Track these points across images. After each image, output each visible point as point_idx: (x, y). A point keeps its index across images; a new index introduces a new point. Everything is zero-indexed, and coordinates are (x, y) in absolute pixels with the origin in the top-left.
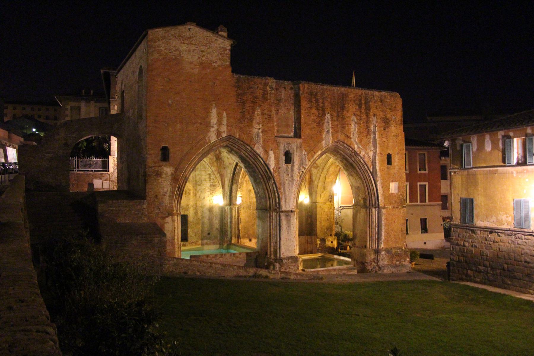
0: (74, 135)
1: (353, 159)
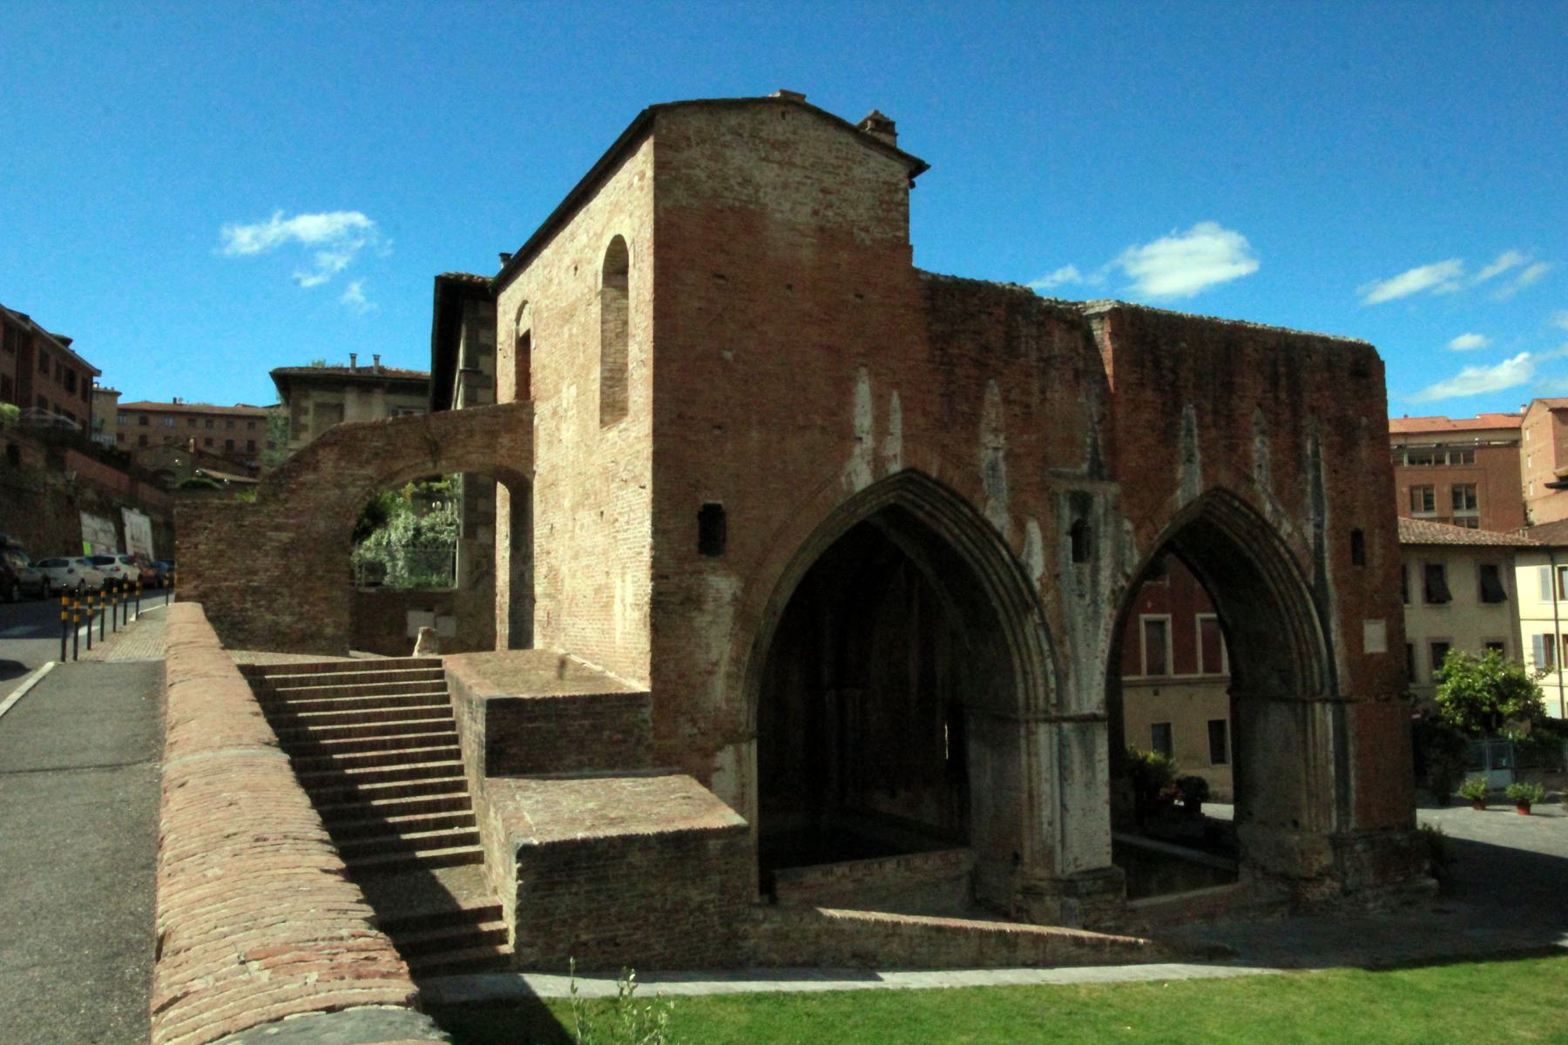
0: (370, 471)
1: (1255, 545)
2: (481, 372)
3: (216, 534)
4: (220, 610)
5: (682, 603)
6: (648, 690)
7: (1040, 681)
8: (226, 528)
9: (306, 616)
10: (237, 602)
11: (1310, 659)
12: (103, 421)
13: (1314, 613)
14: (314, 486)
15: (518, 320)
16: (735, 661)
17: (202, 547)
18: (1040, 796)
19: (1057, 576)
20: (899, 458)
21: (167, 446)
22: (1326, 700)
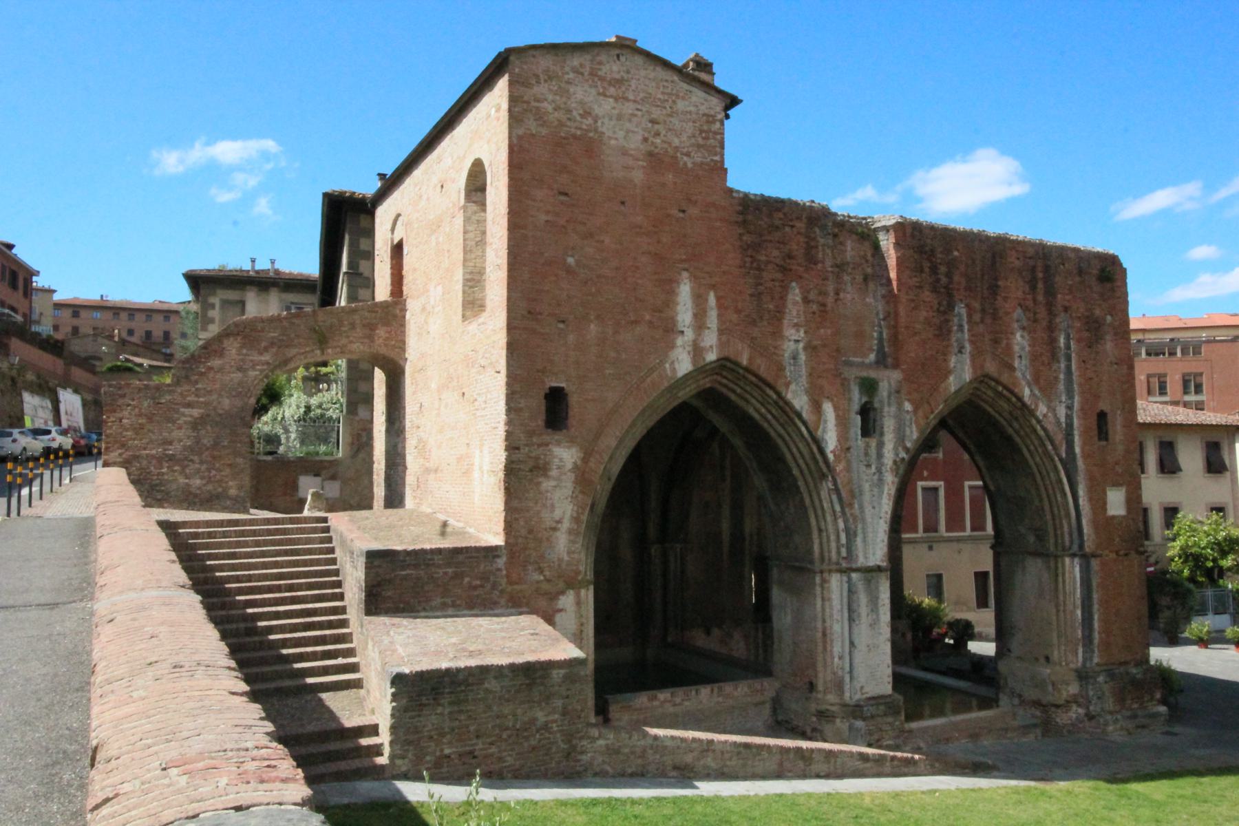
0: (266, 357)
3: (137, 410)
4: (141, 474)
5: (531, 471)
6: (502, 543)
7: (833, 537)
12: (41, 314)
13: (1065, 480)
14: (221, 370)
15: (393, 230)
17: (125, 421)
22: (1073, 555)
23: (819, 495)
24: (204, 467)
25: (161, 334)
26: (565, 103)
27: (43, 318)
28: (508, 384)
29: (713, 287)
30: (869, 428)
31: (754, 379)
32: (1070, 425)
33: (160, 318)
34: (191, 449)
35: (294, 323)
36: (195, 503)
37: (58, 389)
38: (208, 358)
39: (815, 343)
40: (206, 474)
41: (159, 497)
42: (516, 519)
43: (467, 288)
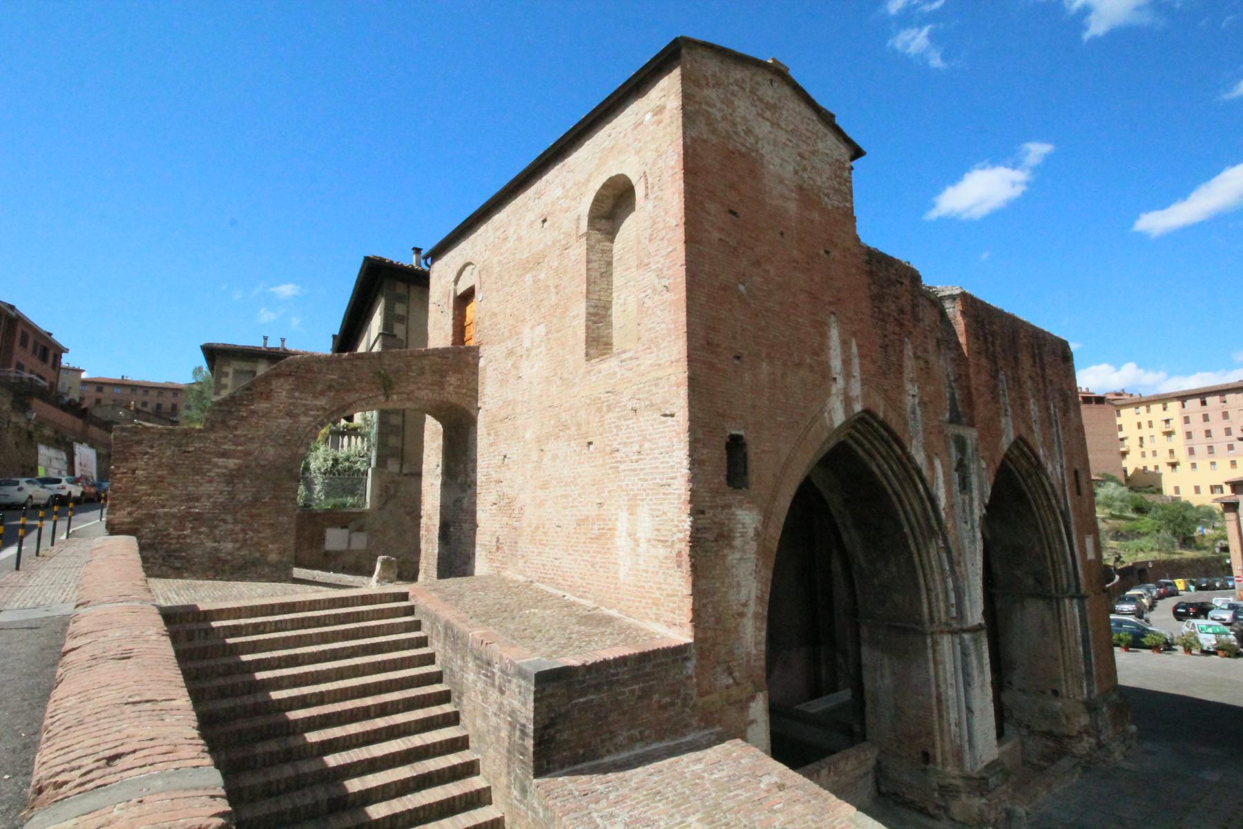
0: (322, 402)
1: (1030, 482)
2: (395, 336)
3: (156, 460)
4: (155, 538)
5: (716, 540)
6: (691, 640)
7: (941, 597)
8: (169, 453)
9: (249, 542)
10: (175, 529)
11: (1059, 565)
12: (70, 388)
13: (1063, 530)
14: (266, 414)
15: (456, 281)
16: (760, 599)
17: (139, 472)
18: (947, 700)
19: (952, 506)
20: (860, 398)
21: (114, 406)
22: (1072, 597)
23: (928, 552)
24: (238, 528)
25: (170, 406)
26: (731, 115)
27: (71, 391)
28: (691, 430)
29: (854, 334)
30: (965, 486)
31: (885, 434)
32: (1063, 480)
33: (170, 394)
34: (224, 508)
35: (356, 366)
36: (224, 572)
37: (75, 443)
38: (251, 402)
39: (926, 399)
40: (241, 536)
41: (178, 565)
42: (705, 605)
43: (590, 323)
